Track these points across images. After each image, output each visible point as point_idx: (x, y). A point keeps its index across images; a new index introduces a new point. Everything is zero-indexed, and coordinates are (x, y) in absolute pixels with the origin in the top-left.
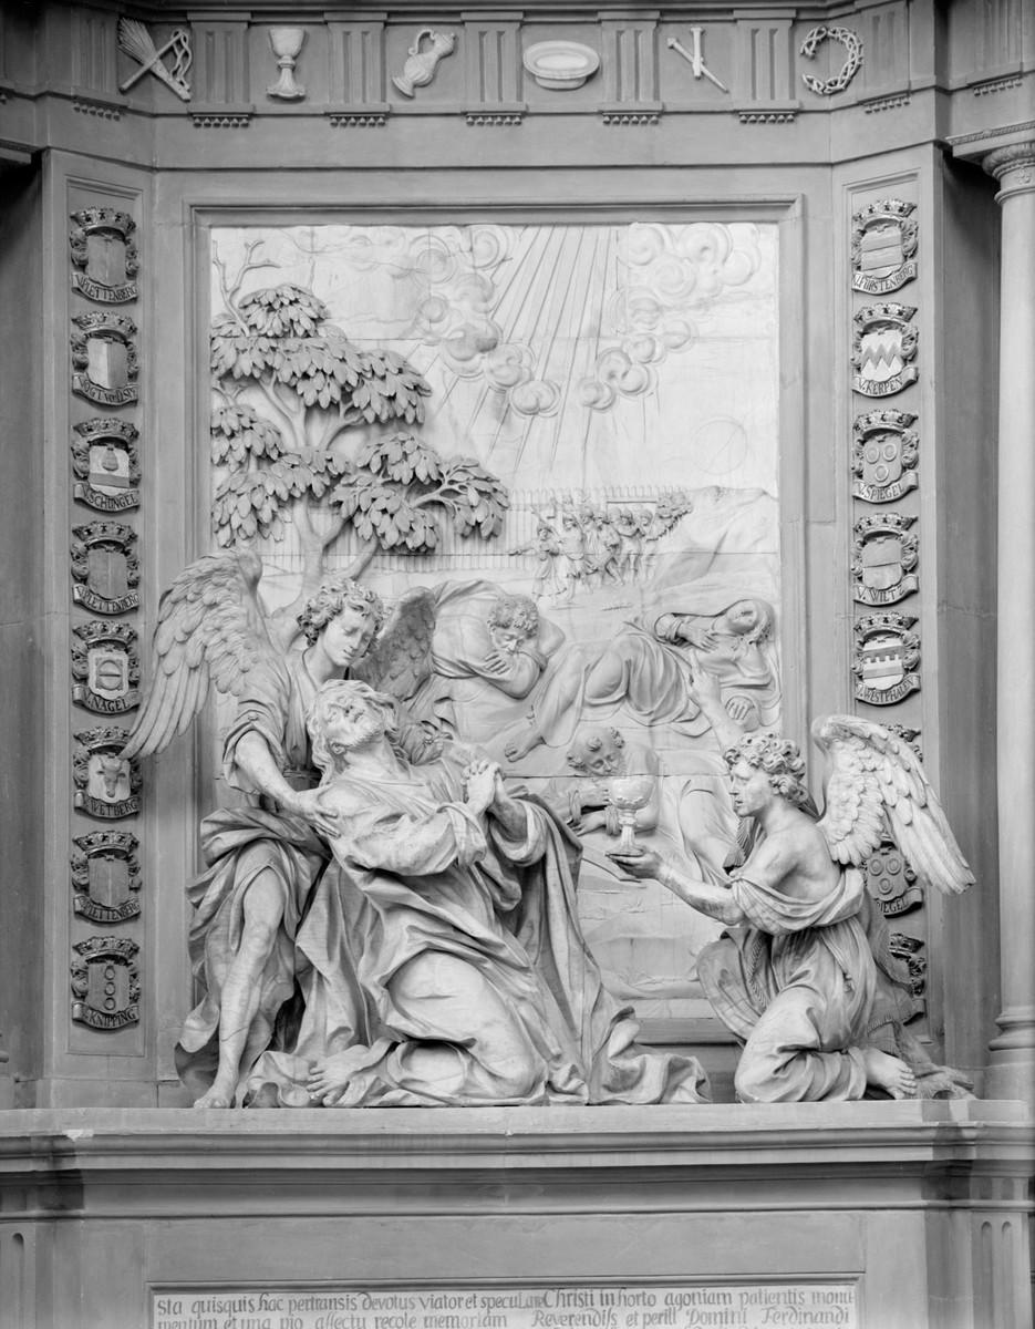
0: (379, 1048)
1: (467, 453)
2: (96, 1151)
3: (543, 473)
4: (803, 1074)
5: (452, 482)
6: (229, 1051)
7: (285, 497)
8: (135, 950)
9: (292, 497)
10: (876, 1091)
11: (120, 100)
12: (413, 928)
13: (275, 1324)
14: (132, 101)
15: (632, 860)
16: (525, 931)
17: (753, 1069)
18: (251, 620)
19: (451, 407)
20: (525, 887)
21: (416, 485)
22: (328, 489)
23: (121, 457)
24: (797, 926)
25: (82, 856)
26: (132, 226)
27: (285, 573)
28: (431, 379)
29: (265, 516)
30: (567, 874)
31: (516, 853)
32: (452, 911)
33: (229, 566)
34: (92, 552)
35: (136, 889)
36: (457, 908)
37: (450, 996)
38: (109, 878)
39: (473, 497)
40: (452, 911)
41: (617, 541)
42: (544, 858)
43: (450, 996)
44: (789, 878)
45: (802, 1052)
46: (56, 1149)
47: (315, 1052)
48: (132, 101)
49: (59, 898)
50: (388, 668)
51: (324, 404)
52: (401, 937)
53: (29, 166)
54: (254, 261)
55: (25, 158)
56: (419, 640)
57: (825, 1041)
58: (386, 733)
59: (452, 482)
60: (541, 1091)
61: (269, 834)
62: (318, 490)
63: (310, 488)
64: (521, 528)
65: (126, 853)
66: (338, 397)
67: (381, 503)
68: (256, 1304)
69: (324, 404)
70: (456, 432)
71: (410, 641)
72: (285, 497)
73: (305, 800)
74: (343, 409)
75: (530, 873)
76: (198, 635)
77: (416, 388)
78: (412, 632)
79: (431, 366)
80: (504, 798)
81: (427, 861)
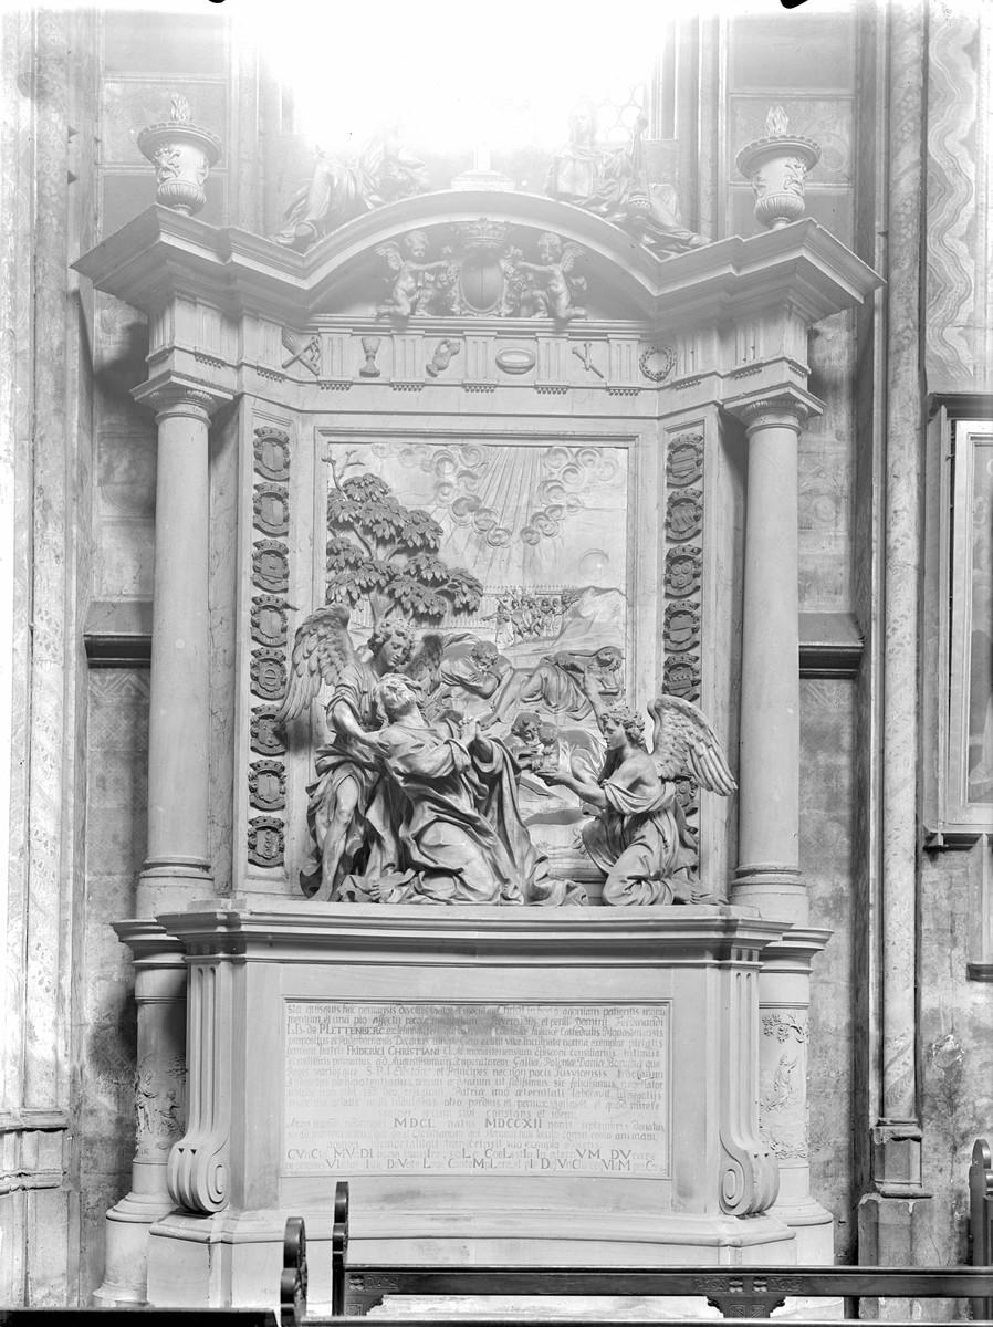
0: (410, 873)
1: (461, 565)
2: (251, 922)
3: (501, 576)
4: (642, 892)
5: (454, 580)
6: (329, 876)
7: (365, 586)
8: (282, 825)
9: (368, 586)
10: (678, 901)
11: (282, 371)
12: (430, 808)
13: (3, 399)
15: (551, 775)
16: (490, 814)
17: (612, 888)
18: (369, 538)
19: (454, 541)
20: (492, 789)
21: (435, 583)
22: (388, 583)
24: (639, 810)
25: (255, 773)
26: (287, 495)
27: (364, 628)
28: (443, 526)
29: (355, 596)
30: (513, 782)
31: (486, 768)
32: (450, 799)
33: (332, 613)
34: (263, 611)
35: (283, 793)
36: (454, 797)
37: (455, 846)
38: (268, 785)
39: (465, 588)
40: (450, 799)
42: (501, 773)
43: (455, 846)
44: (637, 784)
45: (639, 880)
46: (232, 921)
47: (376, 876)
48: (290, 372)
49: (243, 795)
50: (417, 674)
51: (387, 537)
52: (425, 813)
53: (231, 402)
54: (351, 461)
55: (231, 397)
56: (434, 660)
57: (652, 874)
58: (418, 704)
59: (454, 580)
60: (498, 898)
61: (350, 758)
62: (383, 582)
63: (378, 582)
64: (488, 605)
65: (278, 773)
66: (394, 533)
67: (416, 591)
68: (341, 1009)
69: (387, 537)
70: (457, 551)
71: (429, 660)
72: (365, 586)
73: (374, 737)
74: (397, 540)
75: (494, 780)
76: (315, 653)
77: (436, 530)
78: (430, 655)
80: (481, 738)
81: (437, 771)
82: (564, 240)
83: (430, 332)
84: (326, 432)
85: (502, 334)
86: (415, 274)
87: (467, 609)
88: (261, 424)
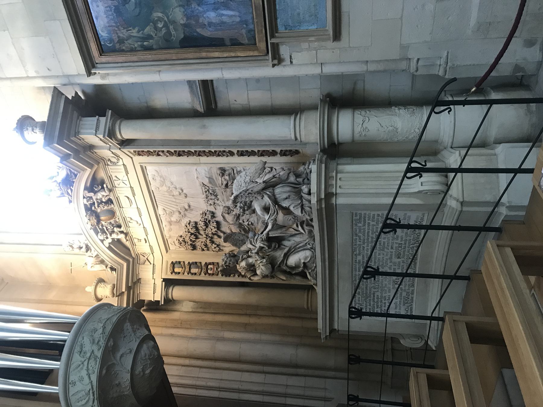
3: (201, 205)
14: (152, 263)
23: (210, 267)
41: (211, 194)
48: (152, 263)
70: (196, 217)
79: (185, 221)
82: (84, 197)
83: (127, 226)
84: (167, 252)
85: (120, 206)
86: (111, 235)
87: (213, 215)
88: (169, 273)
